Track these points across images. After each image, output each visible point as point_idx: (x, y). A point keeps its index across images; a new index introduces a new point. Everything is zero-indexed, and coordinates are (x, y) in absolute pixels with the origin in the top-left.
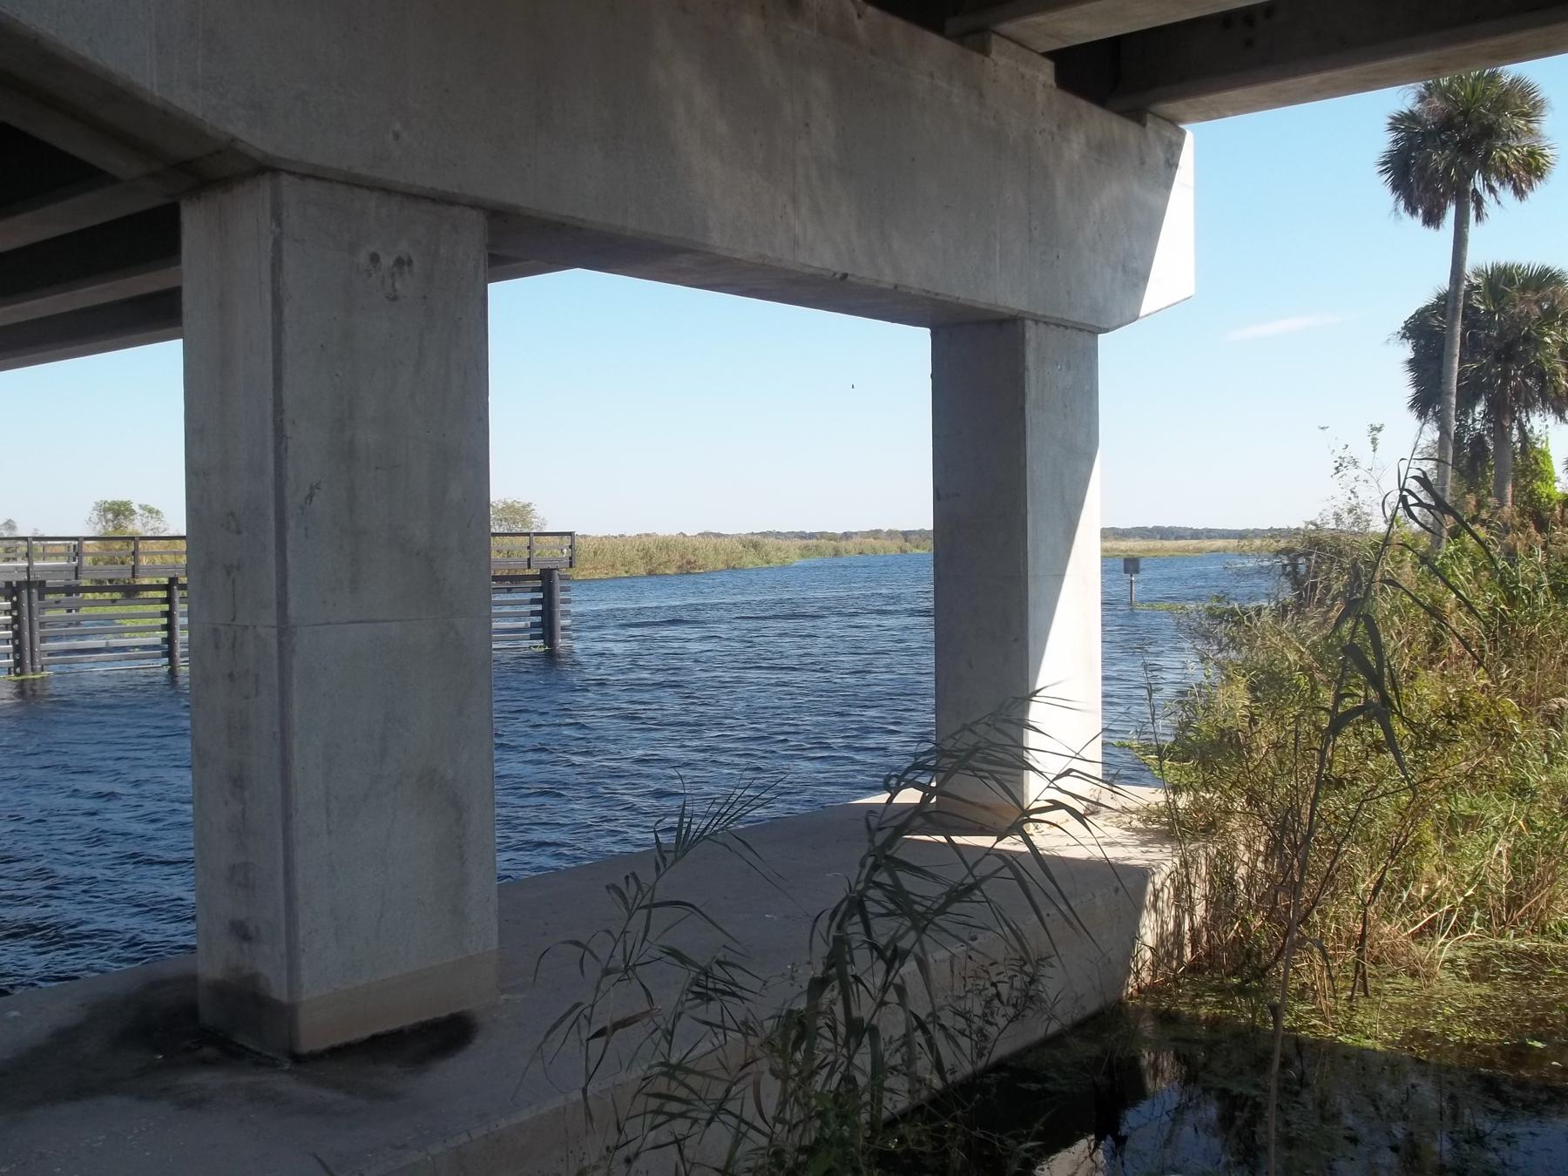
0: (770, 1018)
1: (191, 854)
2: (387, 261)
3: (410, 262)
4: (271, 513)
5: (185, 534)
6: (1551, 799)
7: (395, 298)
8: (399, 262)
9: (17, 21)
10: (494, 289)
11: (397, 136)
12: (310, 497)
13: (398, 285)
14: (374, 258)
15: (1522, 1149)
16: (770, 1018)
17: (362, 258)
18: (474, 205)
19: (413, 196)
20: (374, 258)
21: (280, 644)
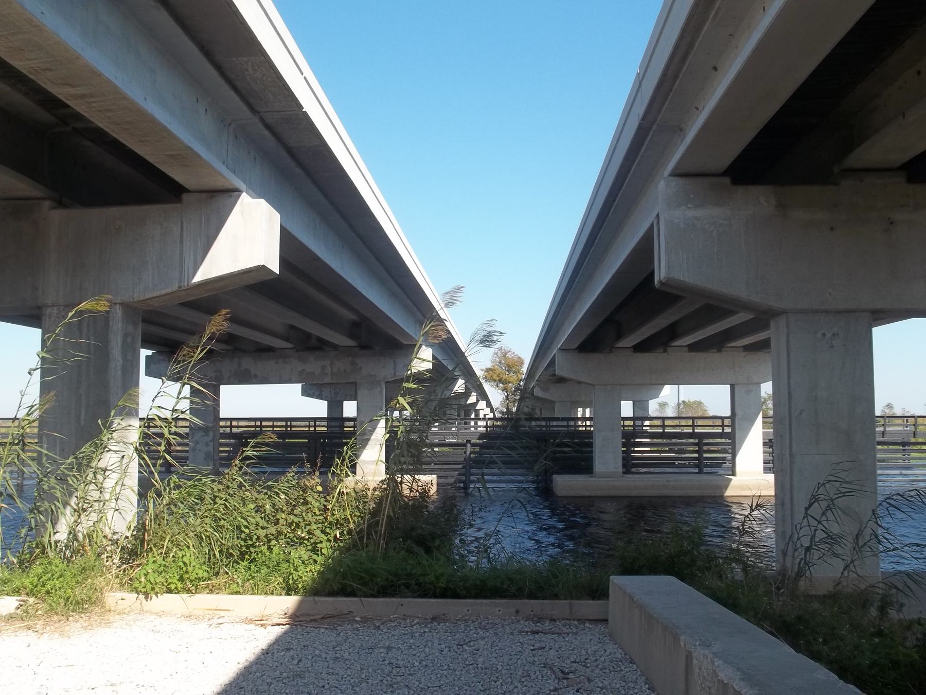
0: (803, 519)
1: (879, 447)
2: (829, 335)
3: (838, 334)
4: (787, 418)
5: (727, 388)
6: (134, 577)
7: (832, 347)
8: (834, 335)
9: (685, 281)
10: (875, 330)
11: (830, 294)
12: (801, 413)
13: (833, 342)
14: (824, 335)
15: (136, 423)
16: (803, 519)
17: (819, 335)
18: (864, 311)
19: (839, 312)
20: (824, 335)
21: (790, 460)
